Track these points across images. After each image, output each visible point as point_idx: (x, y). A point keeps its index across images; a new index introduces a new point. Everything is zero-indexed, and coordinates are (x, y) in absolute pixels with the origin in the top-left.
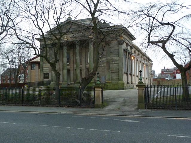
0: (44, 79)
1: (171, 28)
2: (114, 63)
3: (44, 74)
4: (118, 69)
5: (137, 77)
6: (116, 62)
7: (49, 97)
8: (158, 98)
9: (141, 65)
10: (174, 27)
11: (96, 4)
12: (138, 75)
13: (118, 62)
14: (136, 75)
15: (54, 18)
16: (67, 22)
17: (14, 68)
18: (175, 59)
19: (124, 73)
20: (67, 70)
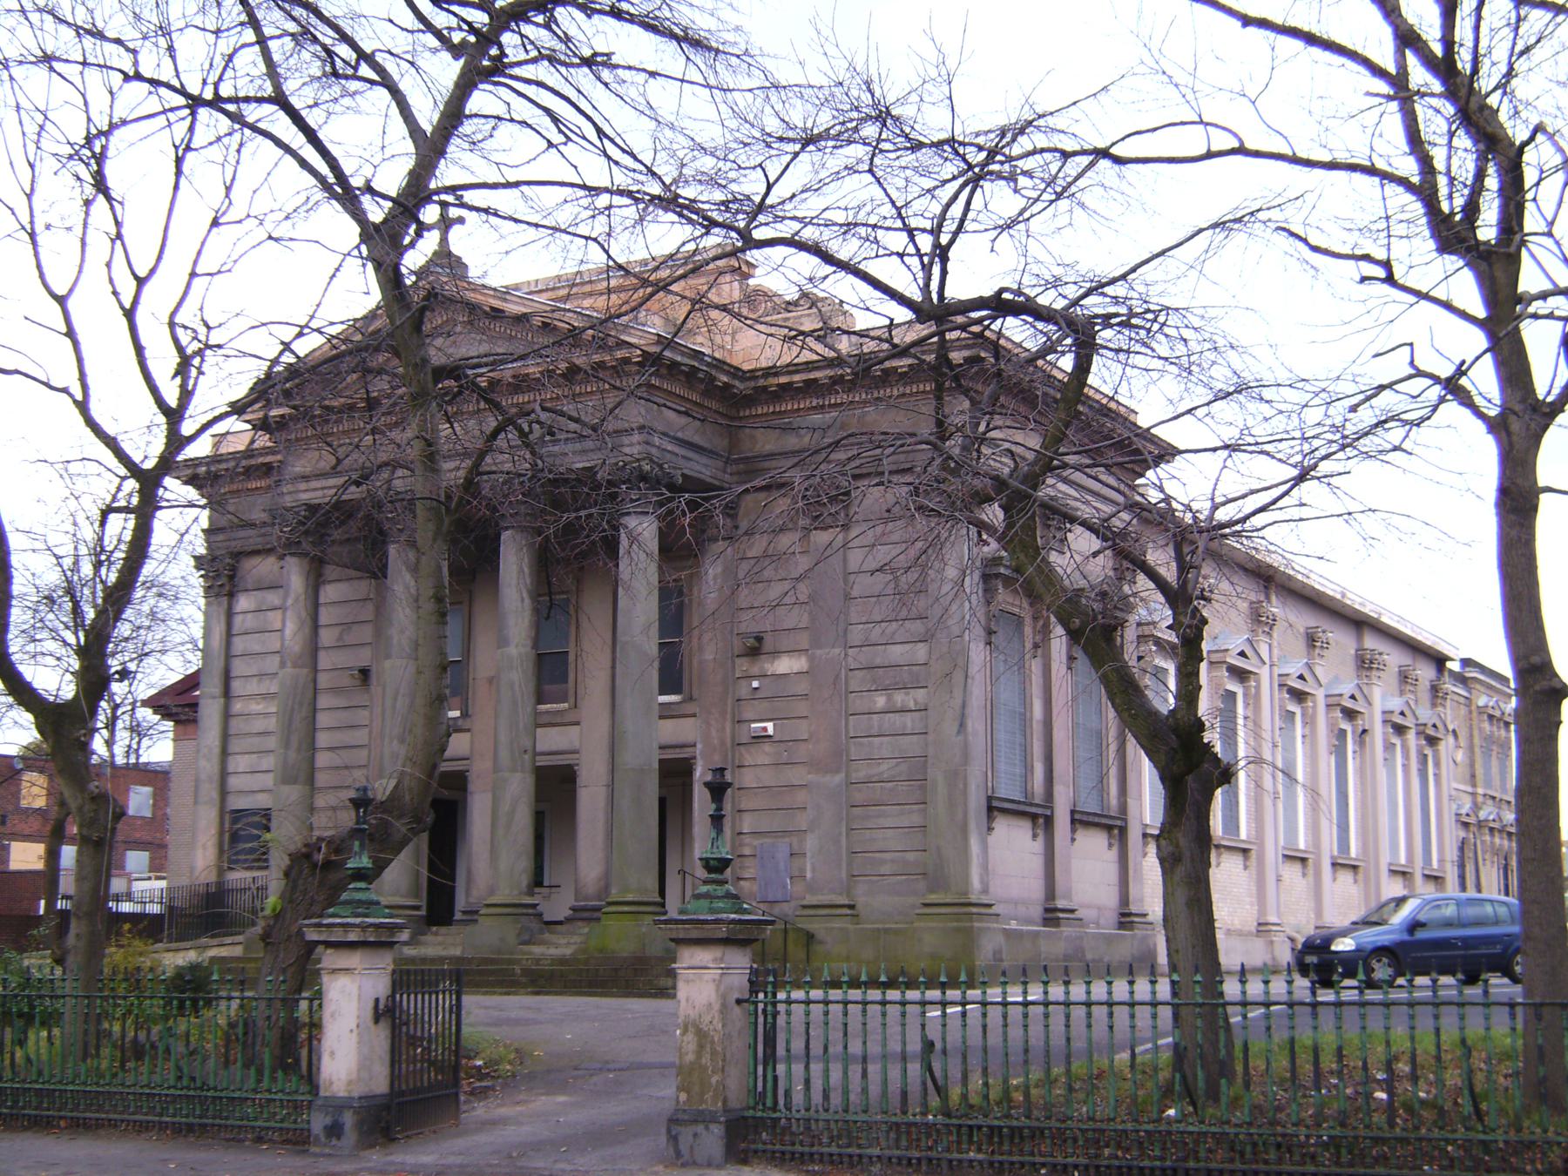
0: (233, 864)
1: (1408, 348)
2: (880, 701)
3: (238, 815)
4: (918, 774)
5: (1296, 868)
6: (899, 698)
7: (1175, 1127)
8: (416, 988)
9: (1406, 755)
10: (1411, 345)
11: (428, 128)
12: (1435, 864)
13: (921, 694)
14: (1329, 846)
15: (111, 281)
16: (808, 383)
17: (120, 760)
18: (157, 524)
19: (976, 802)
20: (530, 780)
